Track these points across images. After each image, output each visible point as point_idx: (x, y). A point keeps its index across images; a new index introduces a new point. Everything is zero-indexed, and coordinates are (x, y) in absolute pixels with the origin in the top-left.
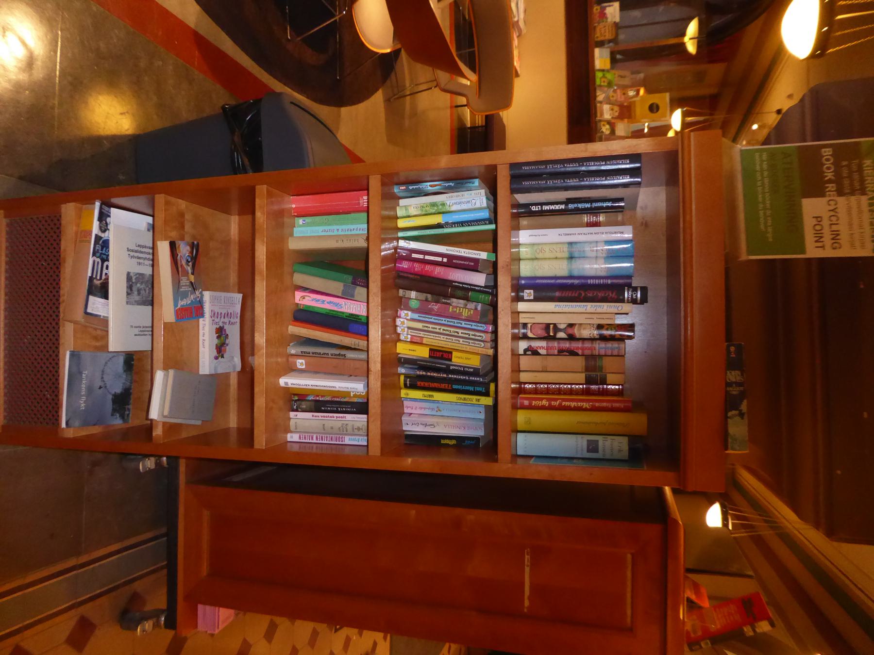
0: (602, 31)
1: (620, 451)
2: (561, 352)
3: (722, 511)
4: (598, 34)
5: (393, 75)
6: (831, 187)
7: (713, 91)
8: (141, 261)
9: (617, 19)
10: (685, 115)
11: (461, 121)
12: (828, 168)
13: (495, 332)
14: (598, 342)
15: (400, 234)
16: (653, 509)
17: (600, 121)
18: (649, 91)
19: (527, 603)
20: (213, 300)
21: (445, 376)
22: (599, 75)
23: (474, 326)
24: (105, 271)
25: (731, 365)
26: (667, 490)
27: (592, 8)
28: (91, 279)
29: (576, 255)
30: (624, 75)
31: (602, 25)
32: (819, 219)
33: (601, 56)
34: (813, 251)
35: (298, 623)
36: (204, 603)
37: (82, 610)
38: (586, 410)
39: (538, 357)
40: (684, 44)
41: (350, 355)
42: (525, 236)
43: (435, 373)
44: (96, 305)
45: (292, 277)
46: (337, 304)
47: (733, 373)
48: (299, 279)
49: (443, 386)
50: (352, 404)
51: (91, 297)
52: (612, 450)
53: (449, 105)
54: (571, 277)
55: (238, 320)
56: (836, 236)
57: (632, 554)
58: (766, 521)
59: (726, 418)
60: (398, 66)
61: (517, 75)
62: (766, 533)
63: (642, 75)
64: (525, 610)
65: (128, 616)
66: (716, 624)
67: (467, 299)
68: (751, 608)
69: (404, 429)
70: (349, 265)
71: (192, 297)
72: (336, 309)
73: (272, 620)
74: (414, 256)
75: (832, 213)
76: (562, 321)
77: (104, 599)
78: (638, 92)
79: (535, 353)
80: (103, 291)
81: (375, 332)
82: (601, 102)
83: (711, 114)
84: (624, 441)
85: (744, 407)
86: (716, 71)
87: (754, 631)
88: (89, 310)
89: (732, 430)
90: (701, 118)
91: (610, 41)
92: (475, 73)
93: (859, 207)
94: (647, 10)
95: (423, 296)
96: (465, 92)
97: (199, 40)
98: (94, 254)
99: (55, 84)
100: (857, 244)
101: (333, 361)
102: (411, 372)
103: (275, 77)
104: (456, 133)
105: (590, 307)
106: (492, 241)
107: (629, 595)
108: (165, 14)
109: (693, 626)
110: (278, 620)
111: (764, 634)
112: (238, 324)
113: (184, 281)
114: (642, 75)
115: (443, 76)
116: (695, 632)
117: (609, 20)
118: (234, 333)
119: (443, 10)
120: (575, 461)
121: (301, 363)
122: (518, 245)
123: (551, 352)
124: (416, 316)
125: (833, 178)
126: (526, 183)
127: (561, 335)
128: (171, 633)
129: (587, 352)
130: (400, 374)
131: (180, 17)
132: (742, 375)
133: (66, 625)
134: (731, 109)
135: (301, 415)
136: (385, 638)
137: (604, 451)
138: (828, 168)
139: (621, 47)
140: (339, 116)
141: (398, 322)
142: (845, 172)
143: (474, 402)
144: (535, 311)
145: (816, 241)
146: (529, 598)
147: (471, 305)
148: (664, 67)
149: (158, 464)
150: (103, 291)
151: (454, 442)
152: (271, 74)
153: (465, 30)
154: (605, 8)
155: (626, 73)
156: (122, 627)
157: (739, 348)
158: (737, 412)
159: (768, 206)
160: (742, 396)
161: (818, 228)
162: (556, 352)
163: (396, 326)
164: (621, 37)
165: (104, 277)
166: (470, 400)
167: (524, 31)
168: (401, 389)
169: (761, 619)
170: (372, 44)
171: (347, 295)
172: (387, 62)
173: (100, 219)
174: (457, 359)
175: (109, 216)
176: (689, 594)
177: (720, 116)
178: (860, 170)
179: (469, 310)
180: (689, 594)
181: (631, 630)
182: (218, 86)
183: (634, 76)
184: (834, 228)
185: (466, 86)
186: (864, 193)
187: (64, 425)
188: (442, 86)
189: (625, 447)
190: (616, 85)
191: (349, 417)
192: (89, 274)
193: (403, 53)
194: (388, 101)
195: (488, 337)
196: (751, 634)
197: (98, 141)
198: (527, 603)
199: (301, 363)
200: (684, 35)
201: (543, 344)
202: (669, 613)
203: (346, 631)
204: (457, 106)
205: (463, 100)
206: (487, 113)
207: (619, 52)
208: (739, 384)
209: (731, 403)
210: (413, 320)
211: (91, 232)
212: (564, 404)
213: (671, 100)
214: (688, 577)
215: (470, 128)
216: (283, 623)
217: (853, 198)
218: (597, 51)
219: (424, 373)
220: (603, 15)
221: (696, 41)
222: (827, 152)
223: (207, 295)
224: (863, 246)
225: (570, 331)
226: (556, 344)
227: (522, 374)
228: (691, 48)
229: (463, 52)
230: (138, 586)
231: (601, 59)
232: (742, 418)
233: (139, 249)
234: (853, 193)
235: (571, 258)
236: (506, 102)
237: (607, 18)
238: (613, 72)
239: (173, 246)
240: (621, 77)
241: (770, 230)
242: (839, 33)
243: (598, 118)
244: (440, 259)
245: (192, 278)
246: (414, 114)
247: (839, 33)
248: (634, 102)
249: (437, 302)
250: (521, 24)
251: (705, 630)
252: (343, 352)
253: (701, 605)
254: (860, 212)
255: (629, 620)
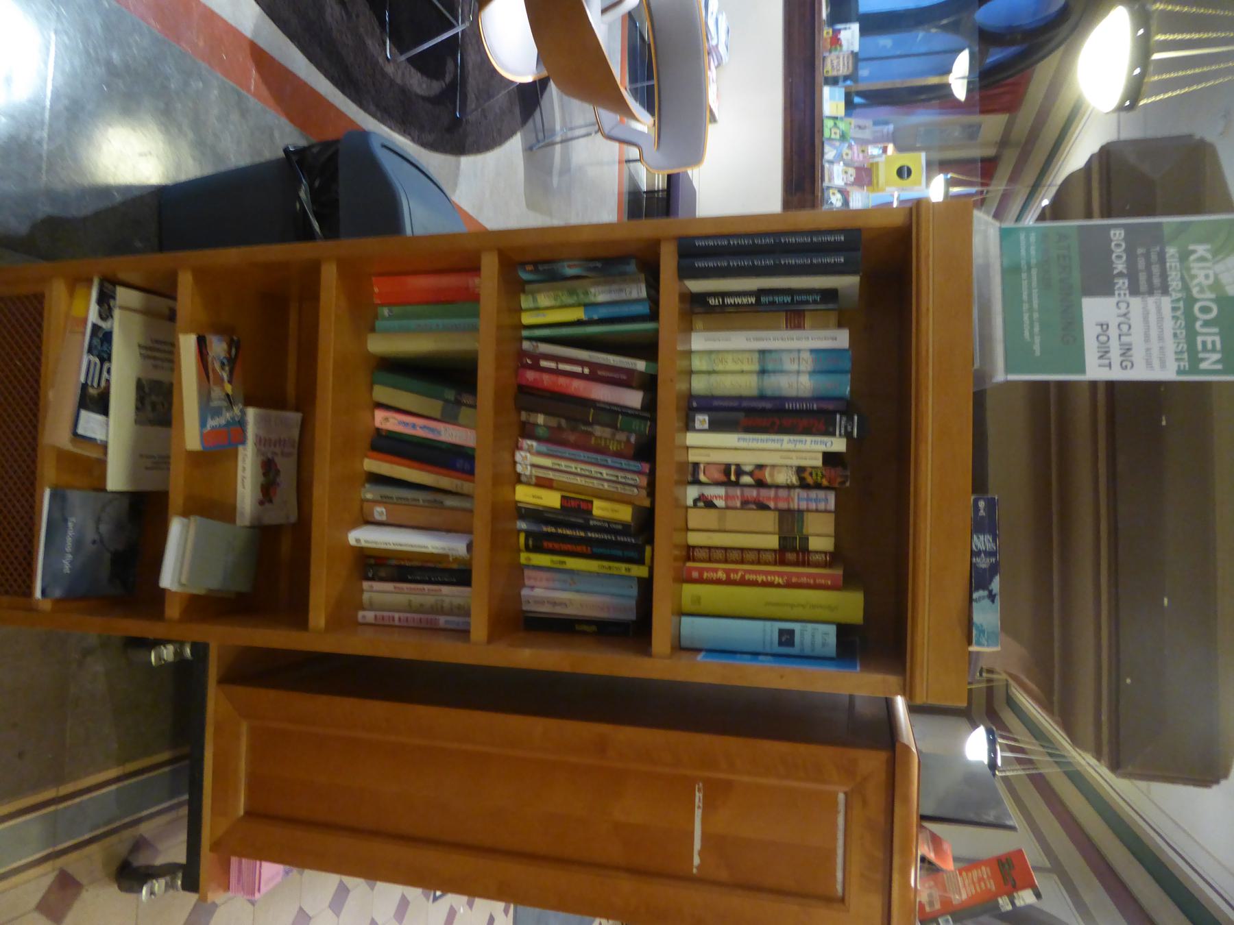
0: (835, 63)
1: (824, 645)
2: (745, 504)
3: (989, 739)
4: (828, 67)
5: (537, 114)
6: (1122, 283)
7: (990, 152)
8: (159, 363)
9: (856, 48)
10: (950, 183)
11: (633, 180)
12: (1119, 257)
13: (652, 475)
14: (797, 490)
15: (525, 333)
16: (883, 733)
17: (829, 188)
18: (900, 149)
19: (697, 860)
20: (262, 422)
21: (582, 534)
22: (828, 124)
23: (624, 463)
24: (105, 374)
25: (979, 526)
26: (900, 703)
27: (821, 31)
28: (84, 387)
29: (770, 367)
30: (864, 124)
31: (834, 54)
32: (1104, 326)
33: (832, 97)
34: (1095, 371)
35: (380, 885)
36: (241, 855)
37: (60, 862)
38: (779, 586)
39: (713, 511)
40: (948, 86)
41: (450, 502)
42: (699, 341)
43: (567, 530)
44: (91, 424)
45: (371, 389)
46: (432, 430)
47: (982, 537)
48: (382, 393)
49: (579, 549)
50: (451, 572)
51: (84, 413)
52: (813, 644)
53: (617, 158)
54: (762, 397)
55: (295, 451)
56: (1126, 350)
57: (846, 793)
58: (1050, 755)
59: (971, 600)
60: (544, 102)
61: (713, 119)
62: (1051, 771)
63: (891, 127)
64: (695, 871)
65: (130, 875)
66: (962, 894)
67: (613, 426)
68: (1010, 871)
69: (524, 608)
70: (449, 377)
71: (228, 415)
72: (430, 436)
73: (341, 882)
74: (544, 363)
75: (1122, 319)
76: (748, 461)
77: (94, 848)
78: (885, 150)
79: (710, 504)
80: (101, 404)
81: (483, 468)
82: (831, 162)
83: (983, 185)
84: (832, 630)
85: (996, 585)
86: (993, 124)
87: (1013, 903)
88: (80, 431)
89: (977, 618)
90: (973, 190)
91: (846, 78)
92: (652, 114)
93: (1159, 310)
94: (897, 36)
95: (553, 422)
96: (640, 143)
97: (259, 56)
98: (90, 351)
99: (44, 108)
100: (1156, 363)
101: (437, 513)
102: (534, 528)
103: (366, 110)
104: (626, 198)
105: (786, 442)
106: (647, 348)
107: (840, 851)
108: (210, 17)
109: (930, 896)
110: (350, 881)
111: (1030, 906)
112: (295, 457)
113: (217, 392)
114: (891, 127)
115: (609, 118)
116: (931, 903)
117: (845, 48)
118: (287, 467)
119: (610, 26)
120: (761, 658)
121: (380, 512)
122: (690, 353)
123: (730, 504)
124: (543, 448)
125: (1125, 271)
126: (700, 264)
127: (746, 479)
128: (192, 898)
129: (782, 505)
130: (519, 531)
131: (231, 21)
132: (994, 540)
133: (39, 882)
134: (1014, 178)
135: (378, 586)
136: (506, 912)
137: (802, 644)
138: (1119, 257)
139: (863, 86)
140: (458, 167)
141: (519, 456)
142: (1141, 263)
143: (623, 572)
144: (708, 445)
145: (1101, 357)
146: (700, 853)
147: (621, 436)
148: (922, 118)
149: (178, 653)
150: (101, 404)
151: (594, 628)
152: (361, 105)
153: (643, 59)
154: (839, 31)
155: (868, 123)
156: (120, 888)
157: (991, 504)
158: (986, 593)
159: (1035, 306)
160: (994, 569)
161: (1103, 338)
162: (738, 504)
163: (515, 463)
164: (864, 72)
165: (103, 384)
166: (617, 569)
167: (725, 59)
168: (519, 551)
169: (1023, 888)
170: (507, 70)
171: (449, 417)
172: (529, 98)
173: (100, 301)
174: (600, 509)
175: (114, 298)
176: (925, 850)
177: (998, 187)
178: (1162, 259)
179: (619, 442)
180: (925, 850)
181: (842, 900)
182: (284, 121)
183: (879, 128)
184: (1124, 339)
185: (642, 133)
186: (1165, 291)
187: (38, 594)
188: (606, 129)
189: (832, 639)
190: (853, 139)
191: (446, 589)
192: (82, 380)
193: (553, 87)
194: (529, 149)
195: (643, 481)
196: (1009, 907)
197: (105, 191)
198: (697, 860)
199: (380, 512)
200: (948, 71)
201: (721, 491)
202: (896, 876)
203: (453, 900)
204: (628, 161)
205: (634, 153)
206: (671, 172)
207: (860, 94)
208: (991, 554)
209: (978, 580)
210: (539, 454)
211: (85, 320)
212: (747, 577)
213: (929, 164)
214: (923, 827)
215: (646, 192)
216: (356, 884)
217: (1151, 301)
218: (826, 90)
219: (553, 530)
220: (836, 41)
221: (965, 81)
222: (1117, 235)
223: (251, 413)
224: (1163, 365)
225: (758, 474)
226: (738, 491)
227: (690, 534)
228: (960, 90)
229: (639, 85)
230: (145, 829)
231: (831, 102)
232: (993, 601)
233: (157, 346)
234: (1151, 292)
235: (763, 372)
236: (696, 156)
237: (841, 45)
238: (849, 120)
239: (202, 343)
240: (860, 127)
241: (1037, 340)
242: (1156, 78)
243: (826, 184)
244: (578, 369)
245: (229, 388)
246: (566, 169)
247: (1156, 78)
248: (877, 163)
249: (574, 430)
250: (722, 49)
251: (946, 903)
252: (439, 497)
253: (944, 865)
254: (1160, 319)
255: (839, 888)
